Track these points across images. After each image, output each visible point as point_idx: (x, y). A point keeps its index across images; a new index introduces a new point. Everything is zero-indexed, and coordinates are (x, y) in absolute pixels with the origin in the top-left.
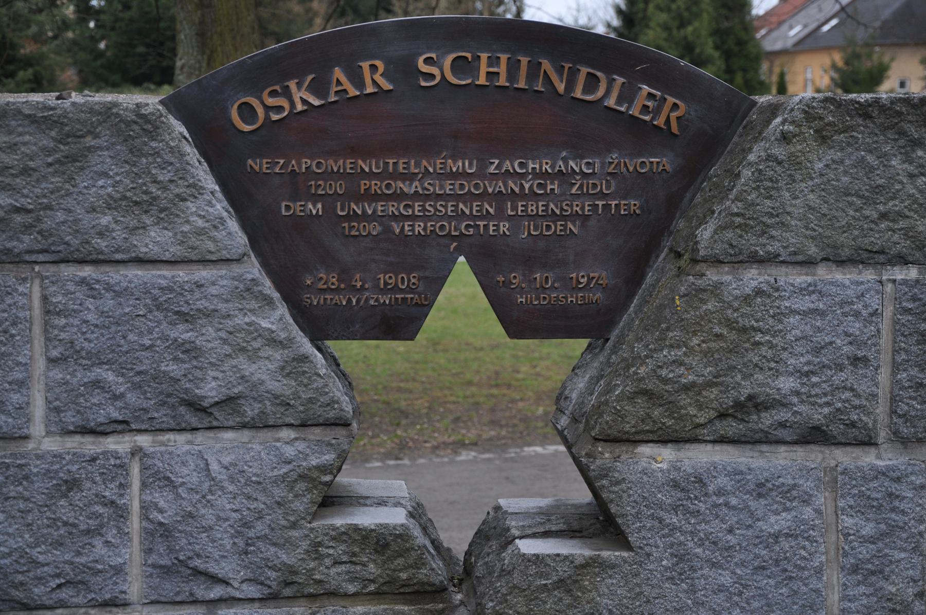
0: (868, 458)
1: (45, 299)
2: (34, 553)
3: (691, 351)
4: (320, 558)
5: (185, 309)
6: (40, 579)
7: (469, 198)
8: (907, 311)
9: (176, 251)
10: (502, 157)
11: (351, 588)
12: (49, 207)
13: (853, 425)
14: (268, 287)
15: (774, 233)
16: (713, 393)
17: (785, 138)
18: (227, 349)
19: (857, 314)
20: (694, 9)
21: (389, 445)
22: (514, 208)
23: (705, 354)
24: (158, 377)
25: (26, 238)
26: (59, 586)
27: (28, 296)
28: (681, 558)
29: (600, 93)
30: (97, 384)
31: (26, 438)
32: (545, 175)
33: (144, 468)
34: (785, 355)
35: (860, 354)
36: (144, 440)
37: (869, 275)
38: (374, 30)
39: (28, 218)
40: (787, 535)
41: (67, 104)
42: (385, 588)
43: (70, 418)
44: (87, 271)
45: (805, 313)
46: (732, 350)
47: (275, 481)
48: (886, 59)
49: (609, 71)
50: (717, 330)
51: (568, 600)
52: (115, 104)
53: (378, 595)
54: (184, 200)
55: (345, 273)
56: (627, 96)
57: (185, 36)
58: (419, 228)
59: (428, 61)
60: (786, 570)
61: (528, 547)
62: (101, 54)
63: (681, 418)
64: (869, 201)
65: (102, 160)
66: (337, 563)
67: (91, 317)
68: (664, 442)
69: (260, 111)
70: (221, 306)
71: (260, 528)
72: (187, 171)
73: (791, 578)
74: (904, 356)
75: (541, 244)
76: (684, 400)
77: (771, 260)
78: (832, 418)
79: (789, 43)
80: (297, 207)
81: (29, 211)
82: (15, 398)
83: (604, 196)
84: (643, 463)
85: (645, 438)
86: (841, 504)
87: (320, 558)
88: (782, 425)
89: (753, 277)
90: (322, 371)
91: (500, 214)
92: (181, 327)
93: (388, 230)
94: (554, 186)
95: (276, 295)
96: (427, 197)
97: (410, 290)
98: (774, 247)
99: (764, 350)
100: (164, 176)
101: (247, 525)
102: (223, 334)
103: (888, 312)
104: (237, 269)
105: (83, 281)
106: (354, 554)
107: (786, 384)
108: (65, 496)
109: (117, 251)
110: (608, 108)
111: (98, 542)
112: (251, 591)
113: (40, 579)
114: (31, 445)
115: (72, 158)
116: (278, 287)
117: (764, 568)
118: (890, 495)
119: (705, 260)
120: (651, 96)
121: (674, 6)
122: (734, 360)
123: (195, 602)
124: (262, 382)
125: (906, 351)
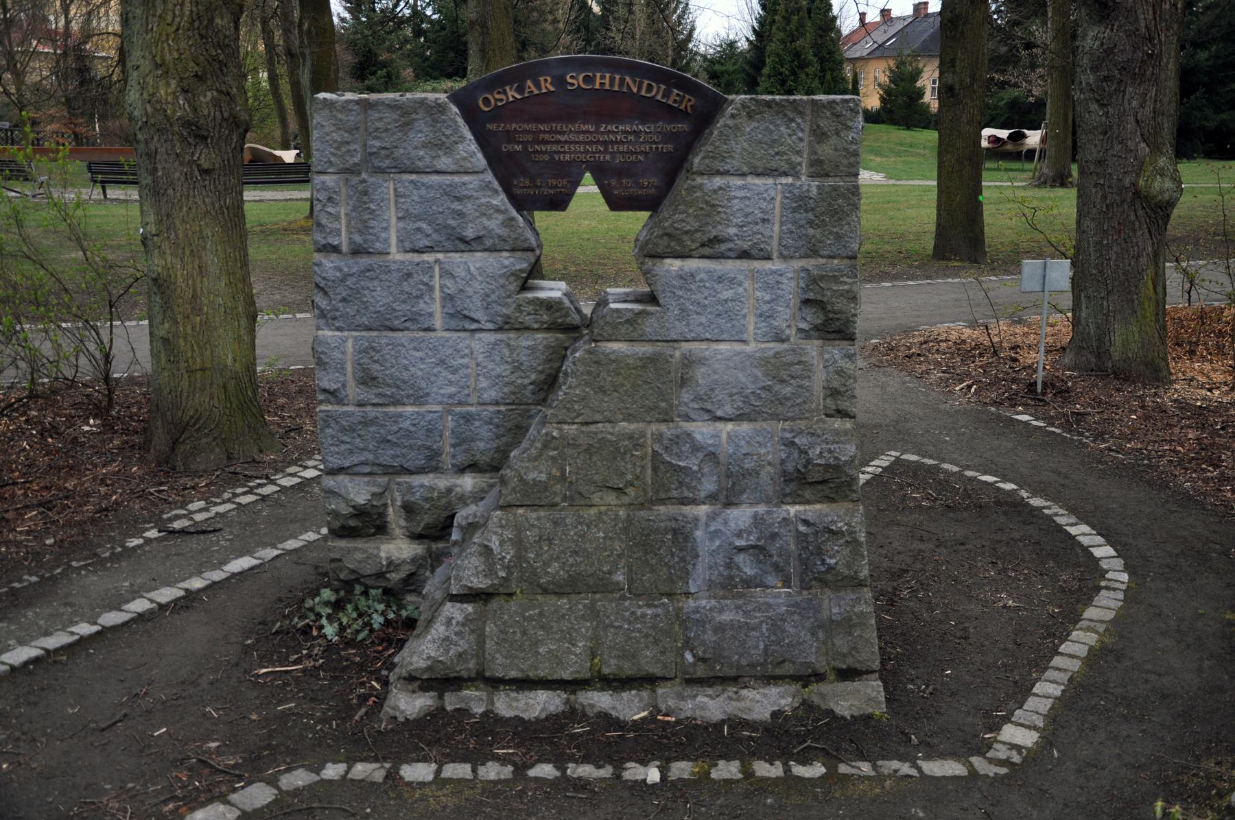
0: (768, 265)
1: (395, 189)
2: (394, 305)
3: (689, 216)
4: (521, 311)
6: (397, 317)
7: (591, 143)
9: (453, 167)
10: (607, 123)
11: (536, 326)
12: (396, 147)
13: (761, 250)
14: (496, 184)
16: (699, 235)
17: (733, 116)
18: (477, 214)
19: (765, 199)
20: (801, 30)
21: (590, 293)
22: (613, 148)
23: (696, 217)
24: (446, 226)
25: (387, 161)
27: (388, 188)
28: (683, 310)
29: (654, 93)
30: (419, 229)
31: (388, 253)
32: (627, 132)
33: (441, 269)
34: (731, 218)
36: (440, 256)
37: (770, 181)
38: (546, 62)
39: (387, 152)
41: (404, 98)
43: (408, 245)
44: (414, 177)
45: (741, 198)
46: (708, 215)
47: (500, 276)
48: (921, 65)
49: (658, 82)
50: (701, 206)
51: (631, 329)
52: (426, 99)
53: (548, 329)
55: (532, 180)
56: (667, 94)
57: (473, 51)
58: (567, 157)
59: (572, 77)
61: (613, 306)
62: (427, 59)
63: (684, 246)
64: (771, 147)
65: (420, 125)
66: (529, 314)
67: (416, 198)
68: (676, 257)
69: (493, 101)
71: (493, 297)
75: (625, 166)
76: (685, 238)
77: (726, 173)
78: (752, 247)
79: (865, 53)
80: (510, 147)
82: (383, 235)
83: (654, 142)
84: (666, 267)
86: (756, 286)
87: (521, 311)
88: (730, 250)
89: (718, 181)
90: (521, 225)
91: (606, 152)
92: (456, 203)
93: (552, 158)
94: (631, 138)
95: (500, 189)
96: (571, 143)
97: (563, 187)
98: (727, 167)
99: (722, 215)
100: (448, 132)
101: (488, 296)
103: (779, 198)
104: (481, 176)
105: (412, 182)
107: (732, 231)
108: (406, 280)
110: (658, 101)
111: (421, 301)
112: (490, 326)
113: (397, 317)
114: (391, 257)
115: (407, 124)
116: (501, 184)
119: (695, 173)
120: (678, 95)
121: (788, 28)
122: (709, 220)
123: (465, 330)
124: (493, 230)
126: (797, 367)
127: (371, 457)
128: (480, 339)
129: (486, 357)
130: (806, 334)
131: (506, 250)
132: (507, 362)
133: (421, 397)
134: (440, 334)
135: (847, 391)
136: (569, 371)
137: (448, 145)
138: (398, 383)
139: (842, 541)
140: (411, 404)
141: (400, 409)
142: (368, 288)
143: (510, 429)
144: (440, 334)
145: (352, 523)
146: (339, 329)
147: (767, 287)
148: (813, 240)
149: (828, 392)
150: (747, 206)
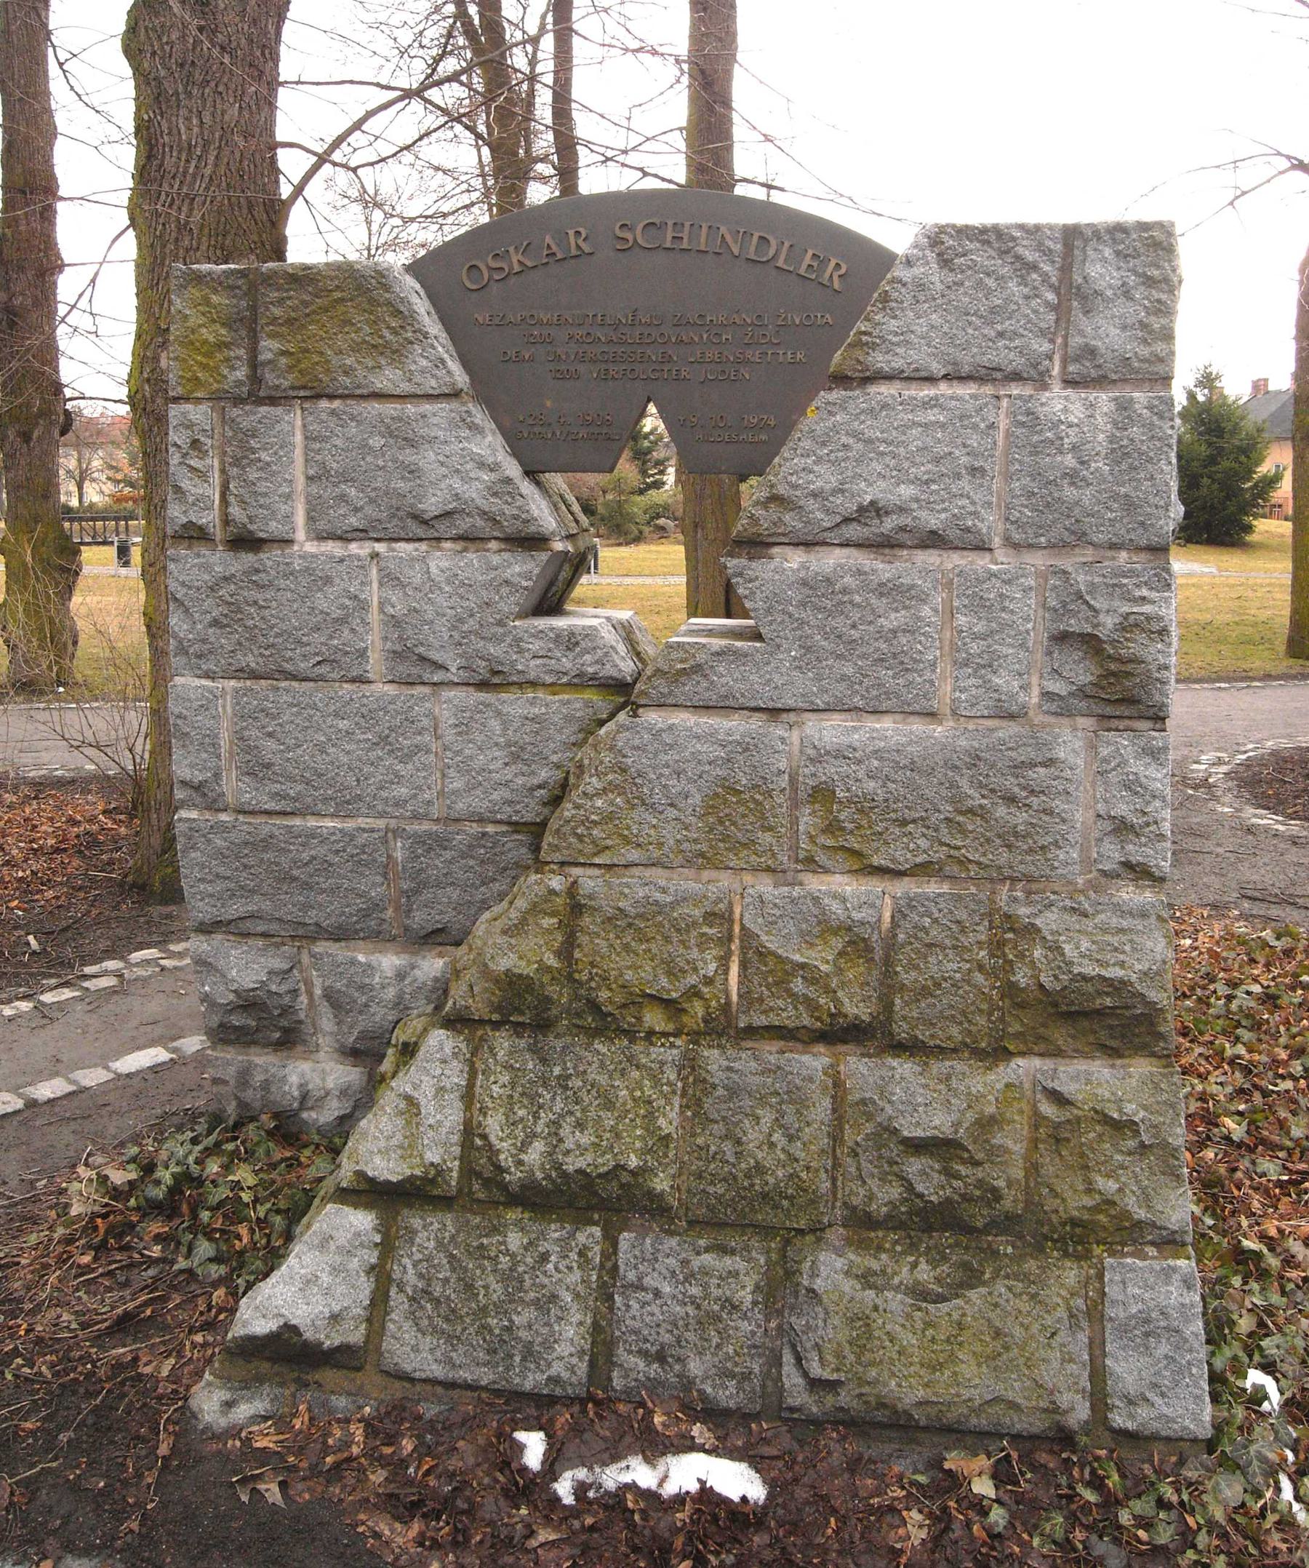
0: (982, 562)
3: (819, 461)
5: (411, 435)
8: (1023, 424)
9: (405, 387)
13: (968, 530)
15: (898, 350)
25: (291, 377)
26: (319, 663)
28: (808, 649)
35: (977, 464)
36: (380, 547)
40: (904, 631)
42: (575, 680)
44: (336, 404)
54: (412, 343)
60: (902, 663)
67: (338, 442)
70: (441, 433)
71: (471, 624)
72: (414, 319)
73: (907, 670)
74: (1017, 467)
81: (292, 354)
82: (284, 508)
85: (778, 540)
87: (521, 651)
88: (903, 529)
101: (461, 621)
102: (441, 458)
103: (1003, 423)
106: (550, 650)
108: (320, 590)
109: (358, 387)
114: (296, 548)
117: (882, 660)
118: (1001, 595)
125: (1020, 462)
126: (1041, 770)
127: (267, 906)
128: (449, 701)
129: (460, 734)
130: (1059, 706)
131: (496, 538)
132: (497, 744)
133: (348, 803)
134: (379, 688)
135: (1148, 824)
136: (586, 762)
137: (395, 346)
138: (307, 775)
139: (1131, 1144)
140: (332, 816)
141: (312, 822)
142: (255, 603)
143: (505, 869)
144: (379, 688)
145: (236, 1020)
146: (208, 675)
147: (979, 605)
148: (1077, 511)
149: (1108, 826)
150: (939, 441)
